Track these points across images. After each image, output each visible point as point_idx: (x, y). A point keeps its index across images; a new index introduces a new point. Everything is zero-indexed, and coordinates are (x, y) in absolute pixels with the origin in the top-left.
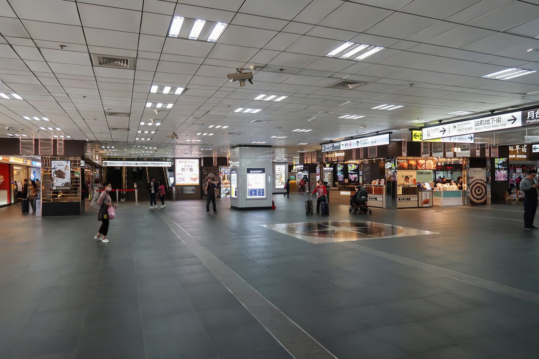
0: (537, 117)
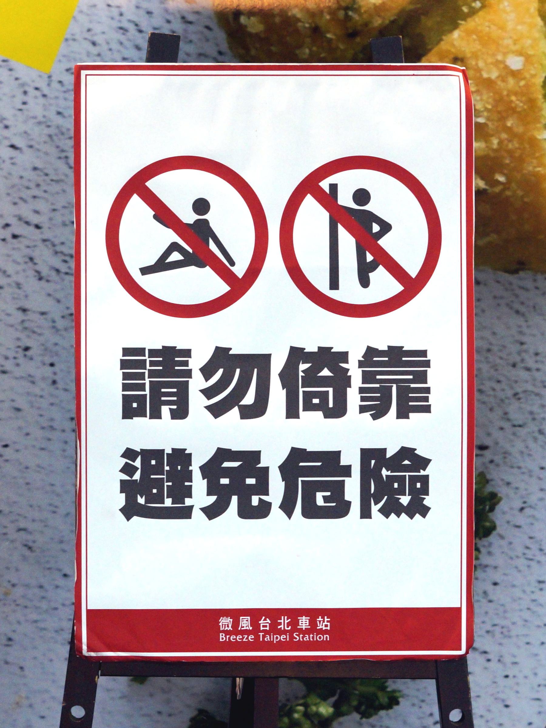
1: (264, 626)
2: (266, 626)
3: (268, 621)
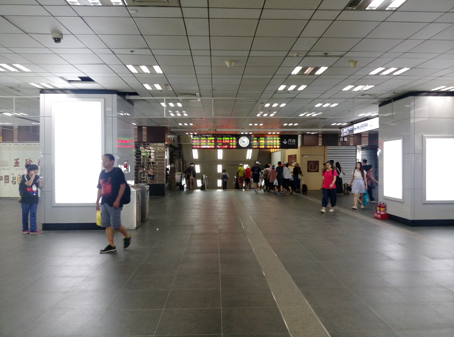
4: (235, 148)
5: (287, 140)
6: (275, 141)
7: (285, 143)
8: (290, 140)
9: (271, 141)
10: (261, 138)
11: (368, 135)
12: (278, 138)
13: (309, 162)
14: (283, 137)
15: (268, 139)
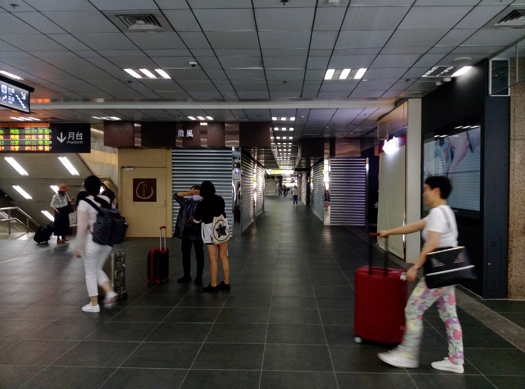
0: (77, 139)
1: (78, 137)
2: (80, 137)
3: (81, 134)
4: (47, 152)
5: (66, 135)
6: (41, 137)
7: (61, 140)
8: (71, 135)
9: (34, 137)
10: (12, 131)
11: (237, 128)
12: (47, 131)
13: (136, 181)
14: (57, 126)
15: (27, 132)
